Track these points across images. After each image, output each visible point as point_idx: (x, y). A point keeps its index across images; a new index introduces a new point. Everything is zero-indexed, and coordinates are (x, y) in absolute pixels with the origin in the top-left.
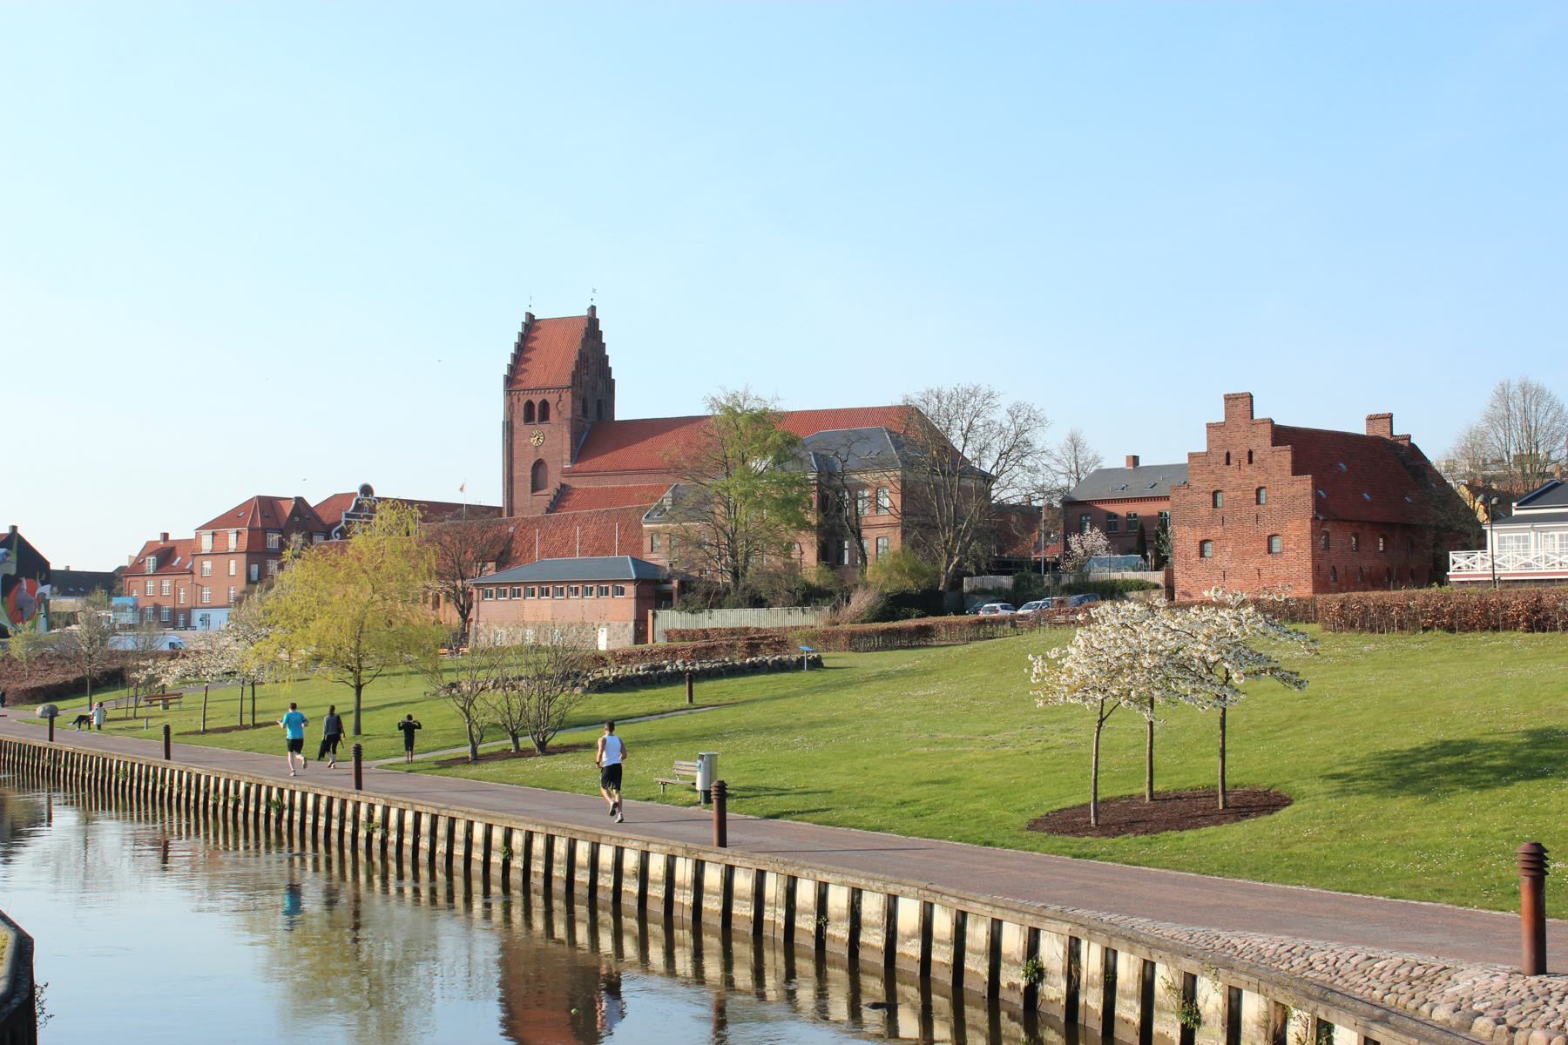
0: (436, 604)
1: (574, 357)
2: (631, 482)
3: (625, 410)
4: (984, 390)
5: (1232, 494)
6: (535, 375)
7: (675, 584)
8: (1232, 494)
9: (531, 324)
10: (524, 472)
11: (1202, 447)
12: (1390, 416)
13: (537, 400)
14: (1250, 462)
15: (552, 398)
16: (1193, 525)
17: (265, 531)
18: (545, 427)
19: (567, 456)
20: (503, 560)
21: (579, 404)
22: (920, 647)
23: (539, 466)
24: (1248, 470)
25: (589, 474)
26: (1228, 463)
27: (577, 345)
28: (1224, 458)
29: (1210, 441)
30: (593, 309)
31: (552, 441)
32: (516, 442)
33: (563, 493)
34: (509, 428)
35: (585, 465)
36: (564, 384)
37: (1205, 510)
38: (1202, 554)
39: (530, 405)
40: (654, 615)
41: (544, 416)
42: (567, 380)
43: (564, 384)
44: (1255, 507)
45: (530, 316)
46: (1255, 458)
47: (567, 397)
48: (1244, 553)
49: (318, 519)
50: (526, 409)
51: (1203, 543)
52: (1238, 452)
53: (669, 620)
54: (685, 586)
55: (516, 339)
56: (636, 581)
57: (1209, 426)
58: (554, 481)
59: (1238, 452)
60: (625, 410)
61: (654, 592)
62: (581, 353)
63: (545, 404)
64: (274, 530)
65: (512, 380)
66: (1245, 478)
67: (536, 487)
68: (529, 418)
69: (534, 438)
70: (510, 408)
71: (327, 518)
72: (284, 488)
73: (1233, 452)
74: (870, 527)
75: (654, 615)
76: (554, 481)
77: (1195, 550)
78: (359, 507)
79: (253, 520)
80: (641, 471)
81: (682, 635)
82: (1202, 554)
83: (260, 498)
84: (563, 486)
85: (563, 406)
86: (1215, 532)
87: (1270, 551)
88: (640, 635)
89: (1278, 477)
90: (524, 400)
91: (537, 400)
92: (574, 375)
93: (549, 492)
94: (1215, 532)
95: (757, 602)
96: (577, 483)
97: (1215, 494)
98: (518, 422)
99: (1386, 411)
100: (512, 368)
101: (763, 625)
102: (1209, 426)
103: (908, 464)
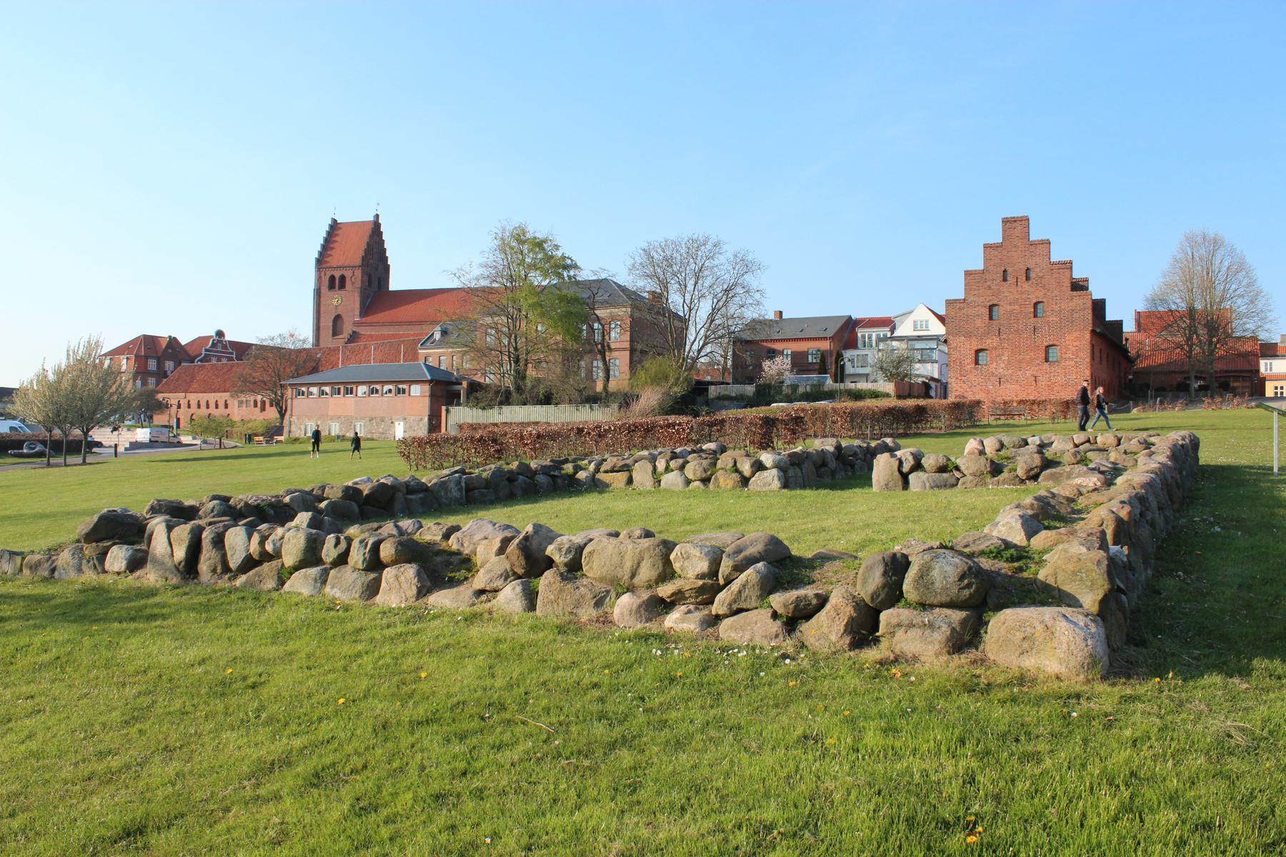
0: (263, 409)
1: (364, 246)
2: (402, 331)
3: (395, 284)
4: (713, 239)
5: (1009, 308)
6: (337, 258)
7: (465, 384)
8: (1009, 308)
9: (335, 226)
10: (327, 323)
11: (979, 265)
12: (1071, 262)
13: (337, 274)
14: (1028, 278)
15: (348, 274)
16: (969, 335)
17: (147, 357)
18: (343, 292)
19: (357, 312)
20: (315, 370)
21: (366, 278)
22: (916, 435)
23: (338, 318)
24: (1026, 286)
25: (372, 324)
26: (1005, 280)
27: (366, 239)
28: (1000, 275)
29: (986, 260)
30: (377, 216)
31: (347, 302)
32: (323, 302)
33: (354, 337)
34: (318, 293)
35: (370, 319)
36: (356, 268)
37: (981, 323)
38: (977, 363)
39: (332, 278)
40: (448, 411)
41: (342, 286)
42: (358, 261)
43: (356, 268)
44: (1033, 320)
45: (334, 221)
46: (1032, 275)
47: (358, 273)
48: (1020, 362)
49: (186, 352)
50: (329, 280)
51: (978, 351)
52: (1016, 269)
53: (460, 415)
54: (474, 387)
55: (319, 249)
56: (430, 381)
57: (986, 247)
58: (348, 329)
59: (1016, 269)
60: (395, 284)
61: (445, 391)
62: (368, 244)
63: (343, 278)
64: (153, 357)
65: (321, 262)
66: (1022, 293)
67: (335, 333)
68: (332, 286)
69: (335, 300)
70: (319, 280)
71: (192, 353)
72: (162, 331)
73: (1010, 270)
74: (624, 349)
75: (448, 411)
76: (348, 329)
77: (970, 359)
78: (214, 345)
79: (140, 347)
80: (410, 323)
81: (473, 427)
82: (977, 363)
83: (145, 336)
84: (354, 332)
85: (355, 279)
86: (990, 342)
87: (1047, 360)
88: (434, 425)
89: (1056, 293)
90: (329, 274)
91: (337, 274)
92: (364, 258)
93: (345, 335)
94: (990, 342)
95: (547, 400)
96: (362, 331)
97: (991, 307)
98: (325, 289)
99: (1067, 259)
100: (321, 253)
101: (551, 420)
102: (986, 247)
103: (634, 307)
